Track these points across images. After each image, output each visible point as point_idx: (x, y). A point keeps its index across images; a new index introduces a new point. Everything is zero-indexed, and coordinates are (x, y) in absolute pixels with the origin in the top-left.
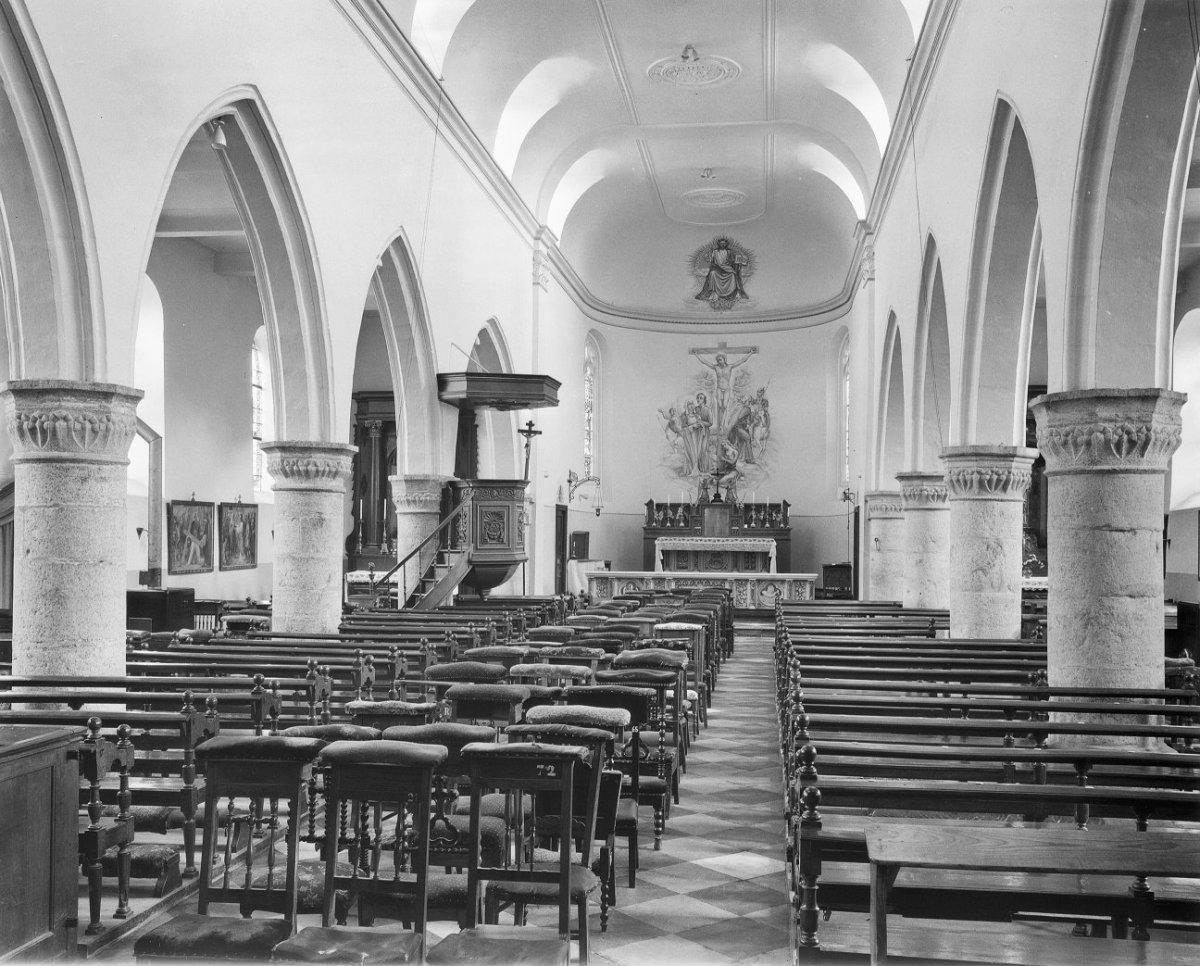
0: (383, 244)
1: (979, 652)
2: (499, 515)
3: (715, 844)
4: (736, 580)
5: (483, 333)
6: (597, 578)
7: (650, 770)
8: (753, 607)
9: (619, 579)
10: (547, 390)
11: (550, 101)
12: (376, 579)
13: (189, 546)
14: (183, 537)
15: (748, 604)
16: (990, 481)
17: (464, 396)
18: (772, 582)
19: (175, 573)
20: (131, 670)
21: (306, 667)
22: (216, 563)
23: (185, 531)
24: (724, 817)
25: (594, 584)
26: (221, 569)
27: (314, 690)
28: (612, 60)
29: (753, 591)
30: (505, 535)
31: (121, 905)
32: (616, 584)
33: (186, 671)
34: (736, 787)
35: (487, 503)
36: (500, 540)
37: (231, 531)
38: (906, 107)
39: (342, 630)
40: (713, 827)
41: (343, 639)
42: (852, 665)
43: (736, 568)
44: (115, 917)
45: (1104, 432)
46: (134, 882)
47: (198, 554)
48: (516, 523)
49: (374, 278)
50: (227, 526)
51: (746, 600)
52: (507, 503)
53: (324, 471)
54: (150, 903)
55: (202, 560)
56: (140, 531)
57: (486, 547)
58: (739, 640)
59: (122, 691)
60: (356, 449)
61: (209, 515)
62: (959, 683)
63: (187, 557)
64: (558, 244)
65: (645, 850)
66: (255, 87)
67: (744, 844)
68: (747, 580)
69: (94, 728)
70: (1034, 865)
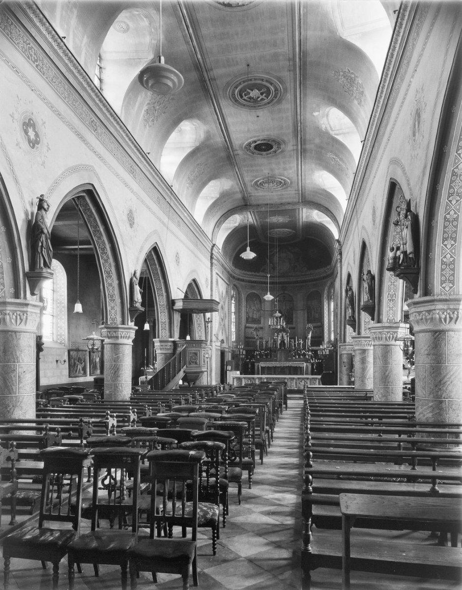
0: (147, 248)
1: (408, 407)
2: (196, 354)
3: (273, 488)
4: (290, 378)
5: (190, 285)
6: (236, 378)
7: (246, 454)
8: (296, 389)
9: (245, 378)
10: (214, 306)
11: (216, 195)
12: (148, 379)
13: (77, 367)
14: (75, 363)
15: (294, 388)
16: (389, 337)
17: (181, 308)
18: (303, 379)
19: (71, 377)
20: (38, 416)
21: (105, 414)
22: (88, 373)
23: (75, 361)
24: (278, 476)
25: (235, 380)
26: (90, 376)
27: (108, 424)
28: (217, 114)
29: (296, 382)
30: (198, 361)
31: (12, 519)
32: (243, 380)
33: (66, 416)
34: (283, 462)
35: (191, 349)
36: (196, 363)
37: (94, 361)
38: (353, 193)
39: (131, 399)
40: (275, 480)
41: (131, 402)
42: (339, 413)
43: (290, 374)
44: (9, 524)
45: (438, 314)
46: (18, 508)
47: (81, 370)
48: (203, 357)
49: (146, 260)
50: (93, 359)
51: (293, 386)
52: (198, 349)
53: (124, 336)
54: (26, 518)
55: (82, 372)
56: (65, 361)
57: (191, 366)
58: (289, 402)
59: (34, 425)
60: (137, 328)
61: (85, 355)
62: (377, 420)
63: (76, 371)
64: (220, 251)
65: (244, 491)
66: (93, 185)
67: (286, 489)
68: (294, 378)
69: (58, 432)
70: (210, 291)
